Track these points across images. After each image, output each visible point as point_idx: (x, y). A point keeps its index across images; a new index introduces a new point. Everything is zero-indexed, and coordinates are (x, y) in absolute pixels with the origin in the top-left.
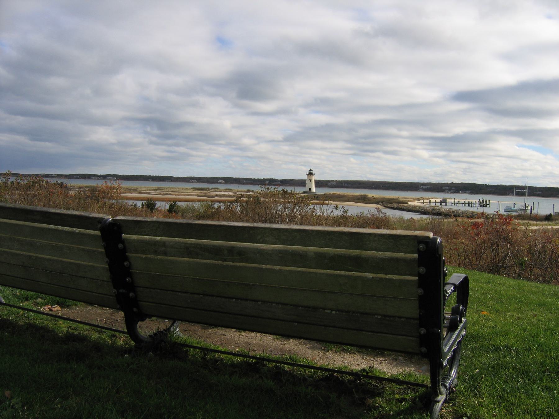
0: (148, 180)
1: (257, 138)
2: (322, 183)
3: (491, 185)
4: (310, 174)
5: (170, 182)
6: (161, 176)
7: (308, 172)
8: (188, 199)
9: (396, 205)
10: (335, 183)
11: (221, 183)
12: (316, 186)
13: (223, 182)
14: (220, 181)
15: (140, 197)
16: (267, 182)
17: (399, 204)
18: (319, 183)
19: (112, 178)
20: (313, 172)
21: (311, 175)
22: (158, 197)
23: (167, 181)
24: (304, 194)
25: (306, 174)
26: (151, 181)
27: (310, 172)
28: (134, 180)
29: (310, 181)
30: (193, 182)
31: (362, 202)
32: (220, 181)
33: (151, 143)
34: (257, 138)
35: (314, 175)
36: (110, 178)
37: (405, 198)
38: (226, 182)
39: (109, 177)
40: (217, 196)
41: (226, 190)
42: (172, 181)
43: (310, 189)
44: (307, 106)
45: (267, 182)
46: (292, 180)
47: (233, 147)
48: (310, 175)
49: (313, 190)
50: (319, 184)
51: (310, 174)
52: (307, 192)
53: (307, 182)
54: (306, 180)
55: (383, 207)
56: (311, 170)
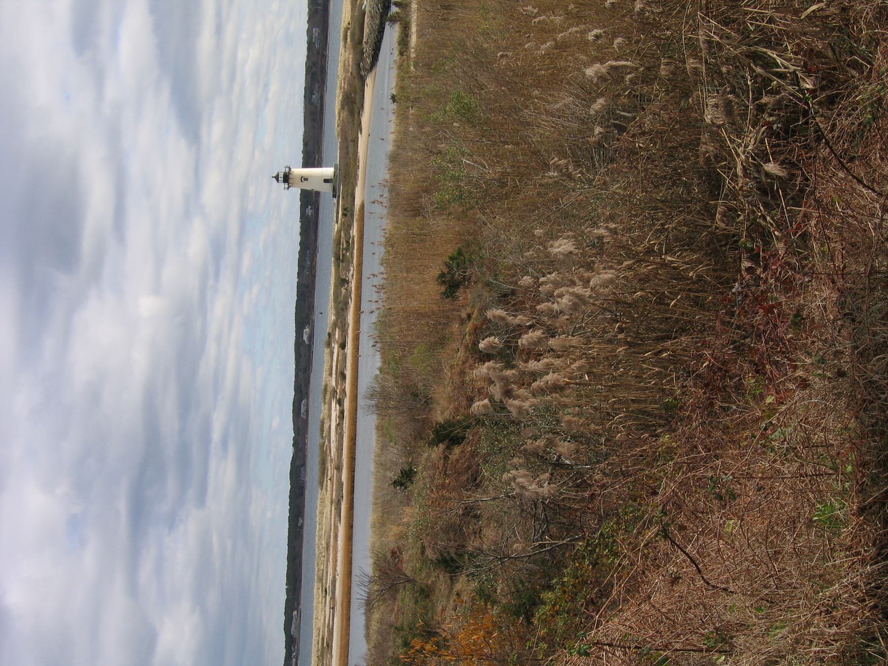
0: (302, 527)
1: (187, 215)
2: (314, 64)
3: (290, 497)
4: (287, 178)
5: (305, 469)
6: (290, 504)
7: (283, 185)
8: (341, 641)
9: (367, 49)
10: (316, 31)
11: (311, 337)
12: (319, 165)
13: (307, 330)
14: (305, 338)
15: (339, 640)
16: (310, 211)
17: (364, 40)
18: (313, 74)
19: (294, 620)
20: (282, 171)
21: (291, 176)
22: (357, 228)
23: (305, 477)
24: (339, 196)
25: (287, 191)
26: (303, 520)
27: (281, 179)
28: (300, 565)
29: (306, 179)
30: (307, 411)
31: (359, 115)
32: (305, 338)
33: (201, 500)
34: (187, 215)
35: (290, 169)
36: (293, 626)
37: (318, 643)
38: (308, 323)
39: (292, 629)
40: (339, 425)
41: (327, 401)
42: (304, 465)
43: (326, 181)
44: (99, 78)
45: (310, 211)
46: (305, 144)
47: (210, 282)
48: (291, 181)
49: (328, 171)
50: (312, 158)
51: (287, 178)
52: (334, 190)
53: (307, 186)
54: (301, 189)
55: (374, 72)
56: (277, 178)
